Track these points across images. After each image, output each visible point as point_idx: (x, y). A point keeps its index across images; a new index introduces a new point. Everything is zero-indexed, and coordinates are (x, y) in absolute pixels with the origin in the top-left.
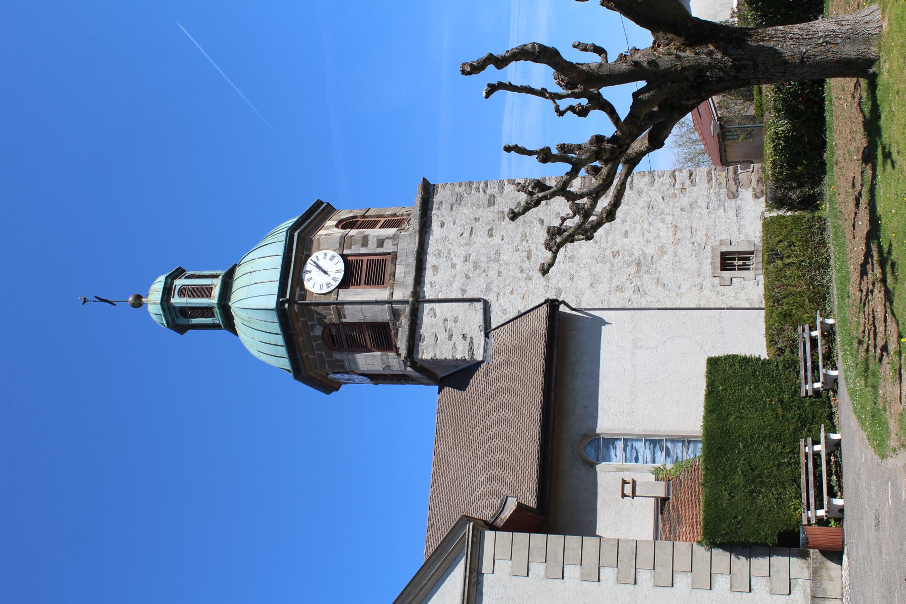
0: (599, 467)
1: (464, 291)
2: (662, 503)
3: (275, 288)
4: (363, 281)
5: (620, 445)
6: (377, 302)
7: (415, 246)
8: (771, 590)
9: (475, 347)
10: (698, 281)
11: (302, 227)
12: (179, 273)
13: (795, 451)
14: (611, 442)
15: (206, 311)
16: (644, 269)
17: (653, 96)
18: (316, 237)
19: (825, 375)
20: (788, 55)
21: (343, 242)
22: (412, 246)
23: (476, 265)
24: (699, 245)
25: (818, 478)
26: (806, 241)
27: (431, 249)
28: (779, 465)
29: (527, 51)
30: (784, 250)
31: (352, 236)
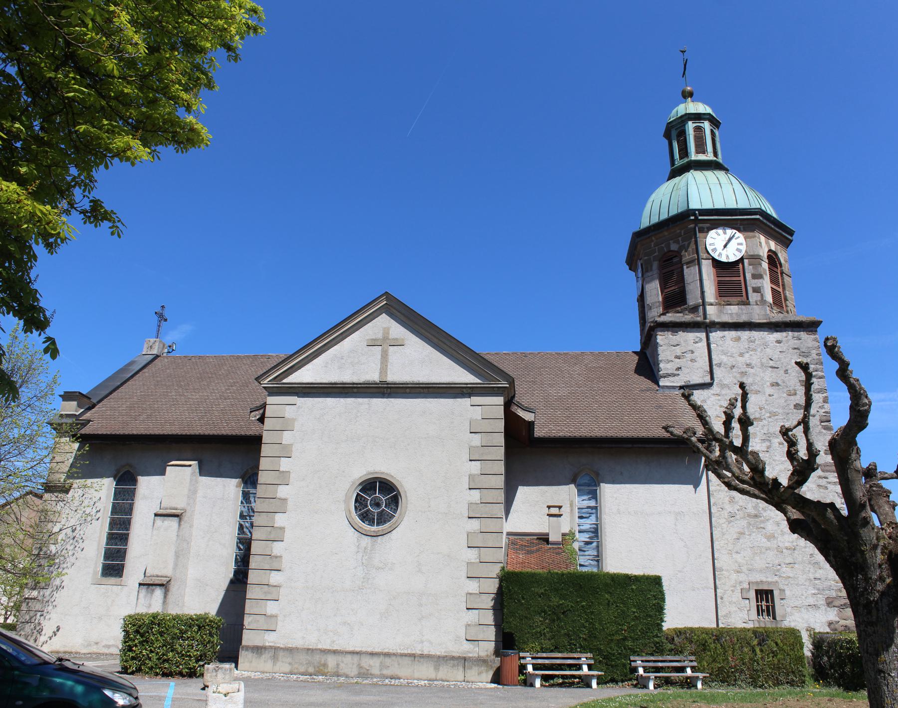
0: (572, 486)
1: (719, 365)
2: (544, 538)
3: (708, 206)
4: (720, 279)
5: (592, 503)
6: (703, 292)
7: (756, 319)
8: (469, 625)
9: (671, 379)
10: (744, 569)
12: (715, 123)
13: (584, 650)
14: (594, 495)
15: (684, 152)
16: (752, 521)
17: (832, 522)
18: (757, 234)
19: (649, 678)
20: (885, 657)
21: (755, 259)
22: (757, 317)
24: (778, 570)
25: (560, 667)
26: (779, 668)
27: (755, 334)
28: (568, 635)
29: (860, 398)
30: (768, 647)
31: (761, 265)
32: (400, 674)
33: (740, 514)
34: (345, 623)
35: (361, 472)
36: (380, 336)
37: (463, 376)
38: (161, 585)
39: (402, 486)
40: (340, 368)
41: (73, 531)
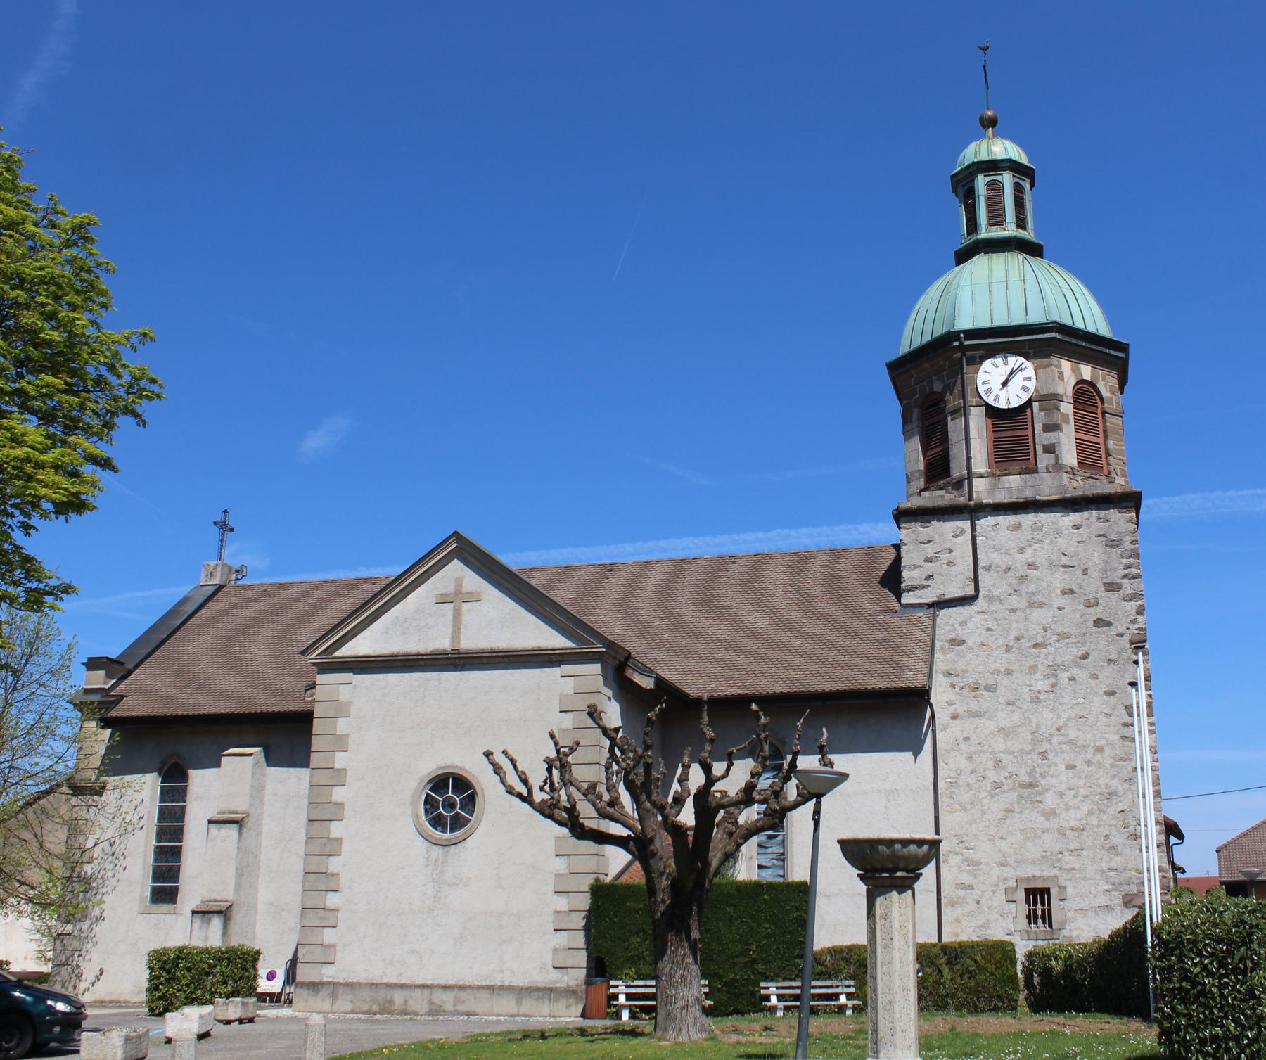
1: (988, 568)
3: (983, 323)
6: (969, 459)
8: (556, 950)
9: (918, 592)
10: (1011, 861)
11: (1067, 339)
15: (973, 226)
16: (1025, 792)
23: (1022, 579)
24: (1058, 860)
26: (979, 992)
27: (1044, 518)
32: (477, 1011)
33: (1008, 784)
34: (413, 952)
35: (429, 766)
36: (451, 589)
37: (554, 640)
38: (219, 912)
39: (478, 782)
40: (403, 634)
41: (112, 845)
